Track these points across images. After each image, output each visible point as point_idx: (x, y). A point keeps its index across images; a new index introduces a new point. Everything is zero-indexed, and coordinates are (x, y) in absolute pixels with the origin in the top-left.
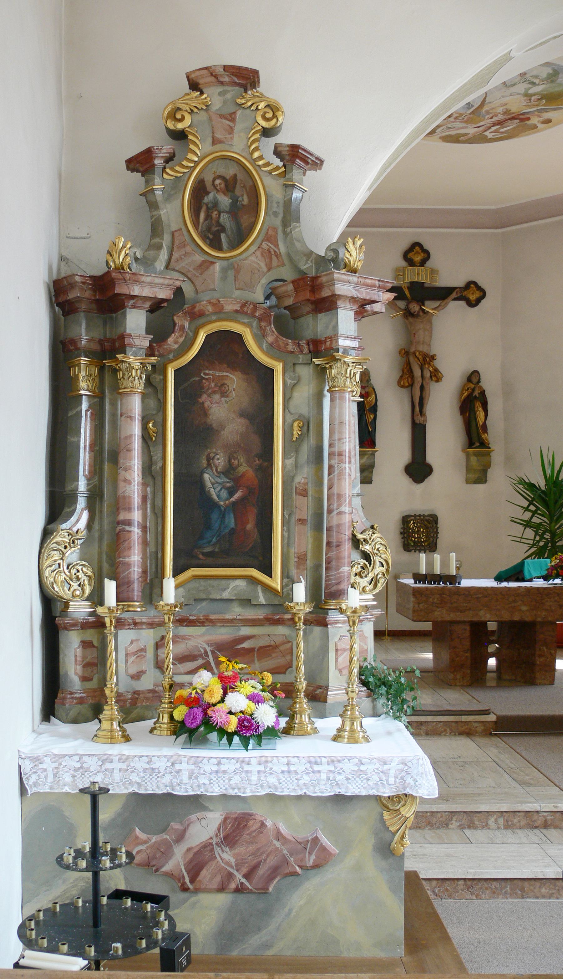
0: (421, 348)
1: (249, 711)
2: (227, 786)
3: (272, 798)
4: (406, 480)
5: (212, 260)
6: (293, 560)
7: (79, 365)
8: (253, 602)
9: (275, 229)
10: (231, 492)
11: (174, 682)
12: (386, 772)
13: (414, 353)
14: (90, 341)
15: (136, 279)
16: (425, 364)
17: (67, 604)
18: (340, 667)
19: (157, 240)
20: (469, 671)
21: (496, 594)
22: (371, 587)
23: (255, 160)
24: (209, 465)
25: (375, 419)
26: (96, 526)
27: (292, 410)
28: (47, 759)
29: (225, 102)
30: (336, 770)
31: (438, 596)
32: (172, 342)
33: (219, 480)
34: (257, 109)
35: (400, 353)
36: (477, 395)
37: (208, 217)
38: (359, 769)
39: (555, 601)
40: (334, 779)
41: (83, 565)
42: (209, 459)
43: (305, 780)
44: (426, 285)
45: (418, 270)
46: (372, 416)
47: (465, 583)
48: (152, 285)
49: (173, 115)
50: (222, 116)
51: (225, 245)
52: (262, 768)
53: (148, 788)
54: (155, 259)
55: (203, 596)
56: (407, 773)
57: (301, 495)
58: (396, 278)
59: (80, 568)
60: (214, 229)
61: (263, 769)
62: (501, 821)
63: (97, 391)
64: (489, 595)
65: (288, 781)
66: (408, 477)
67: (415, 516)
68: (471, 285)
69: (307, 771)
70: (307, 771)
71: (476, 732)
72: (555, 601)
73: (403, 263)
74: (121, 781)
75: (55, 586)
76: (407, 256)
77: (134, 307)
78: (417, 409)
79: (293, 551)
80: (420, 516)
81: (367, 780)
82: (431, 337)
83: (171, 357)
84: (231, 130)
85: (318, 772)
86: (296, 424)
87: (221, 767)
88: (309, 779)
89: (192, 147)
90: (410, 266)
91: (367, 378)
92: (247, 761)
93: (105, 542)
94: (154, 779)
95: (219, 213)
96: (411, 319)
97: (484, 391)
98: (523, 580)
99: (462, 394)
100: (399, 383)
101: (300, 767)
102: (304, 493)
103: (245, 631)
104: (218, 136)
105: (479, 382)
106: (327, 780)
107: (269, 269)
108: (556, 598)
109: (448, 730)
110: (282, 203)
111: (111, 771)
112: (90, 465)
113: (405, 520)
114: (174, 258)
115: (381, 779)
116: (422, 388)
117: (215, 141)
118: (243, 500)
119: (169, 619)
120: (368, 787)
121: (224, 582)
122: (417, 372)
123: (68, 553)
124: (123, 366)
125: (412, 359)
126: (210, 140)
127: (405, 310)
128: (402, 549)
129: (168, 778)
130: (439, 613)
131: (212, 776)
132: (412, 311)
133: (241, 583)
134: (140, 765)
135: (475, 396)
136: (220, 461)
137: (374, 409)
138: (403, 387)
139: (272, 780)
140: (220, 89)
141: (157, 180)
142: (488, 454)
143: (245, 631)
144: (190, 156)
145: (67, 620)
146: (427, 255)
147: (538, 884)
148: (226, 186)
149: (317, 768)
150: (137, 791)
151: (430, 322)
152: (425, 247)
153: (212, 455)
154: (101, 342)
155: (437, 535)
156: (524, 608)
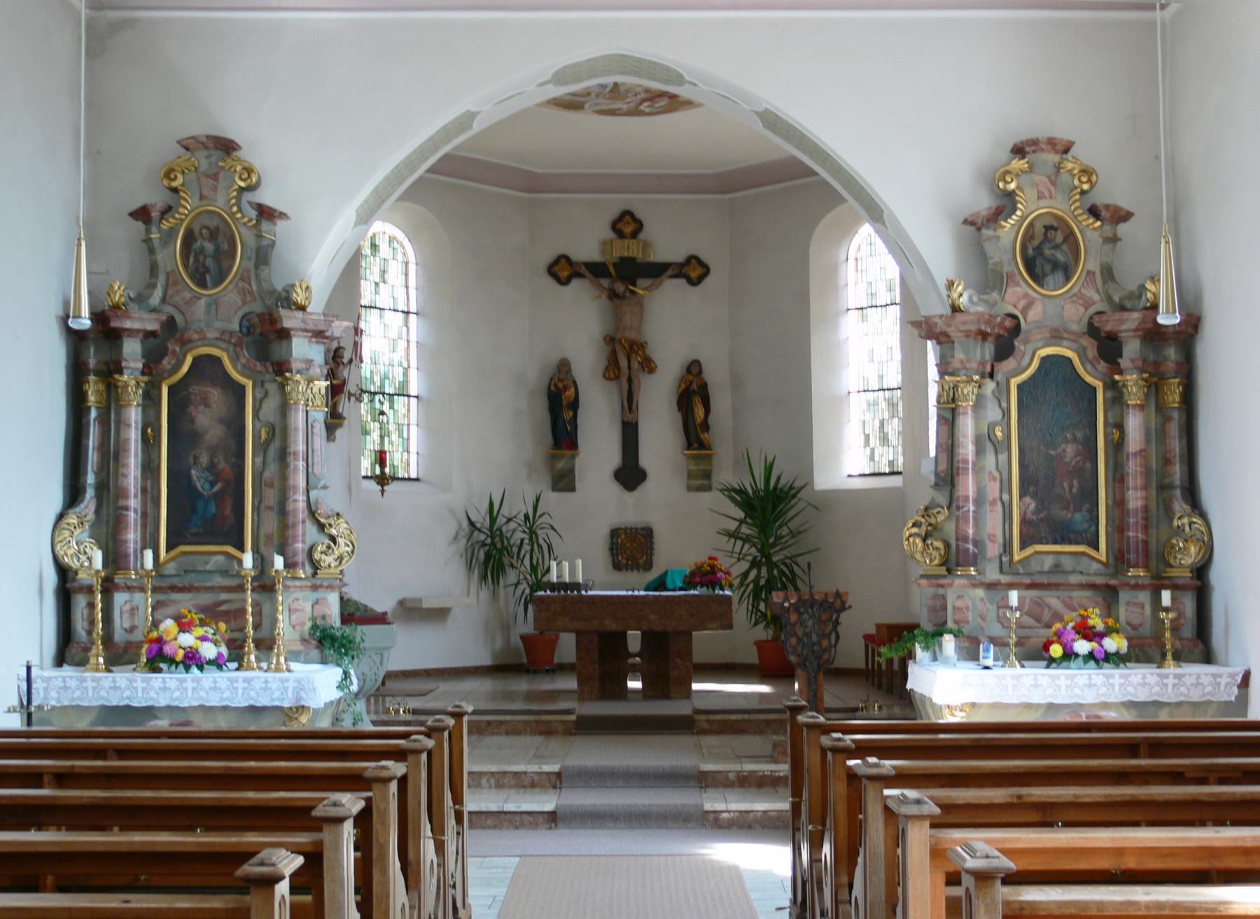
0: (628, 334)
1: (195, 647)
3: (202, 708)
4: (615, 489)
5: (198, 295)
6: (262, 539)
7: (88, 382)
8: (231, 573)
9: (248, 270)
10: (213, 484)
12: (286, 689)
13: (620, 340)
14: (98, 362)
15: (127, 315)
17: (76, 573)
18: (293, 623)
19: (153, 280)
20: (597, 684)
22: (337, 563)
23: (1076, 217)
24: (195, 463)
25: (575, 416)
26: (104, 511)
27: (261, 417)
29: (210, 164)
32: (167, 363)
33: (203, 475)
34: (235, 171)
35: (605, 338)
36: (696, 389)
37: (196, 260)
40: (248, 693)
41: (91, 543)
42: (196, 458)
43: (227, 694)
44: (639, 261)
45: (629, 243)
46: (571, 414)
48: (140, 319)
49: (169, 174)
50: (208, 176)
51: (209, 284)
52: (195, 685)
54: (150, 296)
55: (190, 568)
56: (301, 689)
57: (268, 486)
58: (603, 252)
59: (88, 545)
60: (201, 270)
62: (493, 781)
63: (104, 402)
66: (618, 484)
67: (626, 529)
68: (693, 260)
73: (610, 235)
75: (65, 558)
76: (615, 226)
77: (129, 336)
78: (626, 405)
79: (262, 532)
80: (631, 529)
82: (641, 319)
83: (166, 375)
84: (215, 189)
85: (236, 689)
86: (263, 430)
89: (182, 202)
93: (111, 524)
95: (205, 257)
96: (616, 301)
97: (706, 385)
98: (666, 589)
99: (679, 387)
100: (604, 375)
102: (271, 485)
103: (224, 596)
104: (205, 192)
105: (700, 372)
106: (243, 693)
107: (244, 304)
109: (529, 730)
110: (254, 250)
111: (86, 688)
112: (98, 463)
113: (615, 533)
114: (168, 294)
115: (282, 693)
116: (630, 380)
117: (202, 197)
118: (222, 491)
119: (148, 581)
120: (273, 700)
121: (207, 557)
122: (623, 363)
123: (77, 532)
124: (120, 384)
125: (617, 347)
126: (197, 197)
127: (610, 289)
128: (611, 568)
129: (127, 693)
132: (617, 292)
133: (220, 558)
135: (694, 390)
136: (204, 459)
138: (609, 379)
139: (203, 694)
140: (205, 153)
141: (154, 229)
142: (710, 457)
143: (224, 596)
144: (181, 210)
145: (75, 585)
146: (639, 226)
147: (484, 817)
148: (211, 235)
149: (235, 685)
151: (641, 305)
153: (197, 455)
154: (107, 364)
156: (653, 617)
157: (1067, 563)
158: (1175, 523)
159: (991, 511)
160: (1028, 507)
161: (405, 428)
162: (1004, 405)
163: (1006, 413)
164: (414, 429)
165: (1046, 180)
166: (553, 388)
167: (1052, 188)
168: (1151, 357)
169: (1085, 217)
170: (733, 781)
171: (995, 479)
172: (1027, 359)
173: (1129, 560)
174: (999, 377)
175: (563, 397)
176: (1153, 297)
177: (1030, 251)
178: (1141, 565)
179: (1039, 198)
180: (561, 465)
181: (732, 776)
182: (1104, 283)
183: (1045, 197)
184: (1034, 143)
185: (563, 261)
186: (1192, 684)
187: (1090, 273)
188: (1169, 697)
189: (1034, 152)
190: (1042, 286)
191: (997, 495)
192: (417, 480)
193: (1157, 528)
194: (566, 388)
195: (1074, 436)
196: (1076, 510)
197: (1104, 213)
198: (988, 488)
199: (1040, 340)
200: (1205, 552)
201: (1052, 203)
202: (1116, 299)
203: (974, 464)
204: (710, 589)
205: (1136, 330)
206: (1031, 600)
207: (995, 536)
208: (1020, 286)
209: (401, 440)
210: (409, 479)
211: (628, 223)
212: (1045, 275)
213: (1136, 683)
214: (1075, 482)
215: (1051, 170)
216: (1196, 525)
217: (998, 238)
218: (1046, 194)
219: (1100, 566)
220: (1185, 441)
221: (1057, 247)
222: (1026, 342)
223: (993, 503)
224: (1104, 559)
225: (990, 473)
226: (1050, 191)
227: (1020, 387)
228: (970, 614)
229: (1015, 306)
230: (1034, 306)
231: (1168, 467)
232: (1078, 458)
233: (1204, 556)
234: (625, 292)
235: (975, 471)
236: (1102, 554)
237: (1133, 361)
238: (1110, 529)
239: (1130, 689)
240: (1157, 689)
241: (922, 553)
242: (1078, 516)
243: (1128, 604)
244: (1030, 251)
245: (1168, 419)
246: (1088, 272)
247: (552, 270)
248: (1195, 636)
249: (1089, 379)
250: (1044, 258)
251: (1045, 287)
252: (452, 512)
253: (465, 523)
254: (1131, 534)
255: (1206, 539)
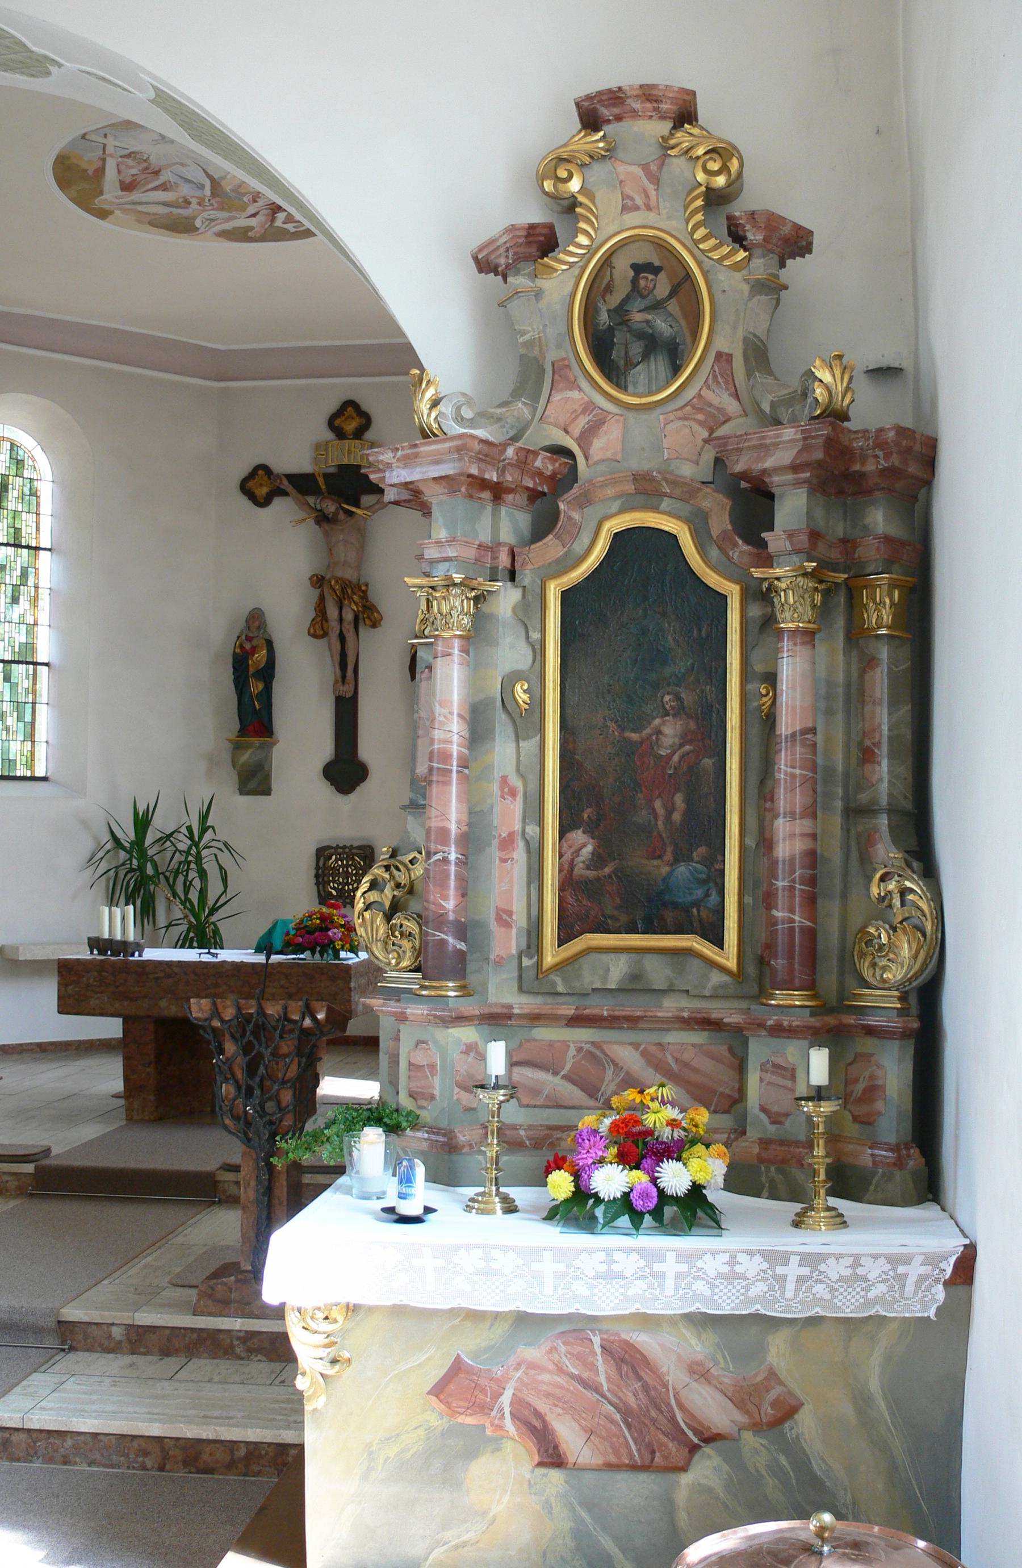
0: (339, 573)
2: (622, 1297)
4: (325, 790)
11: (504, 1124)
16: (345, 599)
20: (152, 1098)
21: (186, 974)
23: (696, 243)
28: (795, 1260)
30: (692, 1271)
31: (96, 974)
38: (732, 1271)
39: (282, 987)
46: (261, 686)
47: (151, 954)
53: (724, 1305)
58: (316, 460)
61: (686, 1270)
64: (176, 974)
65: (730, 1291)
69: (640, 1273)
70: (640, 1273)
71: (7, 1190)
72: (282, 987)
73: (330, 435)
74: (796, 1295)
76: (332, 423)
80: (345, 847)
81: (867, 1290)
85: (660, 1276)
87: (612, 1267)
88: (645, 1287)
90: (339, 439)
91: (257, 624)
92: (658, 1256)
94: (734, 1291)
96: (326, 526)
101: (873, 1270)
108: (282, 982)
113: (322, 853)
116: (342, 638)
122: (332, 612)
130: (97, 1002)
131: (717, 1283)
134: (834, 1270)
137: (267, 673)
138: (314, 636)
146: (366, 421)
150: (763, 1312)
151: (362, 533)
152: (364, 407)
155: (317, 880)
157: (657, 972)
158: (875, 891)
159: (504, 861)
160: (577, 852)
161: (28, 708)
162: (535, 636)
163: (539, 651)
164: (42, 711)
165: (638, 171)
166: (238, 650)
167: (651, 188)
168: (840, 529)
169: (726, 250)
170: (120, 1342)
171: (513, 793)
172: (585, 540)
173: (774, 972)
174: (527, 576)
175: (250, 662)
176: (826, 394)
177: (604, 317)
178: (797, 983)
179: (625, 209)
180: (245, 757)
181: (117, 1333)
182: (749, 374)
183: (637, 208)
184: (615, 97)
185: (260, 472)
186: (841, 1279)
187: (724, 358)
188: (788, 1308)
189: (619, 118)
190: (622, 387)
191: (518, 827)
192: (44, 779)
193: (844, 896)
194: (254, 649)
195: (678, 698)
196: (676, 861)
197: (754, 236)
198: (497, 810)
199: (616, 498)
200: (928, 957)
201: (651, 218)
202: (766, 407)
203: (464, 764)
204: (317, 955)
205: (794, 468)
206: (579, 1050)
207: (510, 913)
208: (580, 389)
209: (21, 725)
210: (33, 779)
211: (351, 418)
212: (630, 365)
213: (713, 1273)
214: (679, 799)
215: (651, 153)
216: (911, 897)
217: (539, 294)
218: (639, 201)
219: (726, 978)
220: (905, 710)
221: (656, 306)
222: (585, 501)
223: (507, 843)
224: (732, 964)
225: (504, 779)
226: (647, 196)
227: (566, 596)
228: (436, 1081)
229: (566, 431)
230: (605, 428)
231: (868, 767)
232: (688, 748)
233: (925, 965)
234: (336, 513)
235: (463, 779)
236: (729, 957)
237: (791, 535)
238: (748, 900)
239: (700, 1287)
240: (760, 1288)
241: (386, 943)
242: (682, 870)
243: (763, 1068)
244: (604, 317)
245: (870, 663)
246: (719, 355)
247: (246, 487)
248: (909, 1138)
249: (713, 579)
250: (630, 330)
251: (630, 388)
252: (85, 824)
253: (106, 837)
254: (779, 914)
255: (929, 927)
